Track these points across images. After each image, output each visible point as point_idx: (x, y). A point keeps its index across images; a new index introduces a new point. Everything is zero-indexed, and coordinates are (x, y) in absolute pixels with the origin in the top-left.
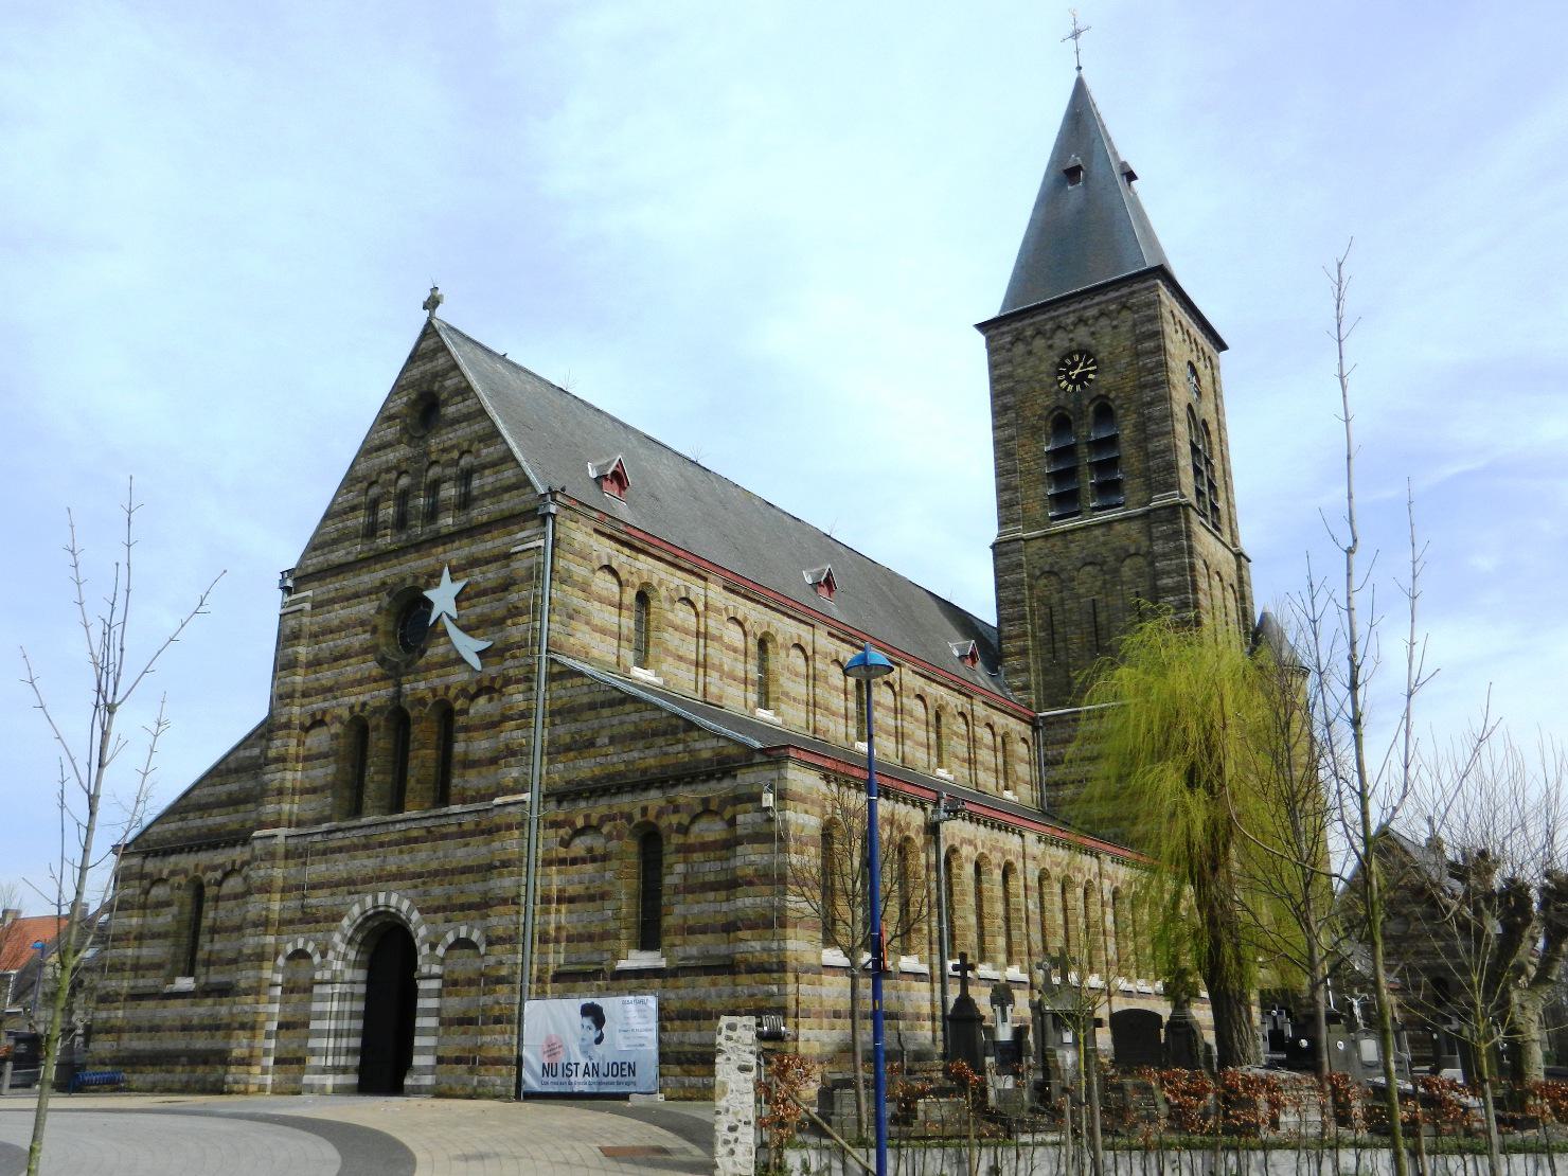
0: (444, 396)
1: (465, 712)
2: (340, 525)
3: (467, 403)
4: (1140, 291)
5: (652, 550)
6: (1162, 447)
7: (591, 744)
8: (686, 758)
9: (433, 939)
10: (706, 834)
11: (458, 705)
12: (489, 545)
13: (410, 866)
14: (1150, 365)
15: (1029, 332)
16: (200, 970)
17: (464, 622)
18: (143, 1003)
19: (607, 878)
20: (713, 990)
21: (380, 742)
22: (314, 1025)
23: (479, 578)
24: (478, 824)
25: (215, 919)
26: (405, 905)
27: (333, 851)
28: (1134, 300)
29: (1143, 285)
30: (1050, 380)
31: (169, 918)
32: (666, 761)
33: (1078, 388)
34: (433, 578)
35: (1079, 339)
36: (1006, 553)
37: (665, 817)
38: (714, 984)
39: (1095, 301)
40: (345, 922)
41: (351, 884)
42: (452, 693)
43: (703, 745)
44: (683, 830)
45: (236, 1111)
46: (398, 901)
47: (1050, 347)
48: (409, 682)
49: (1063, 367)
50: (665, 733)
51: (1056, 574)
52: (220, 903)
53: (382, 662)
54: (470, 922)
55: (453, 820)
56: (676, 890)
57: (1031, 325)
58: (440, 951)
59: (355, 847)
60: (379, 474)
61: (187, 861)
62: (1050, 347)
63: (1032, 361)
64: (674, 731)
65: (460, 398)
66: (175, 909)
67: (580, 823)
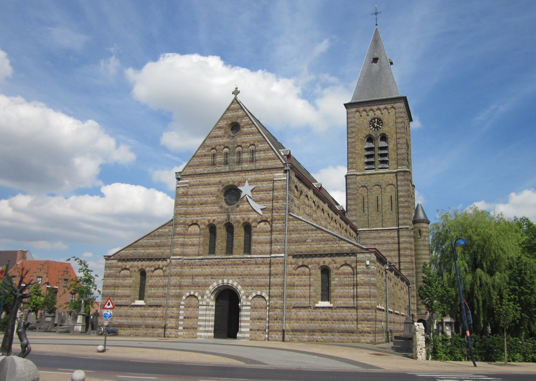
1: (256, 227)
2: (200, 160)
6: (402, 153)
8: (339, 248)
9: (247, 294)
11: (253, 224)
12: (263, 176)
14: (400, 127)
16: (146, 298)
17: (254, 198)
18: (122, 308)
21: (221, 233)
22: (199, 318)
23: (260, 185)
32: (332, 249)
34: (242, 183)
35: (378, 114)
36: (351, 178)
40: (211, 287)
41: (212, 276)
43: (345, 245)
44: (338, 268)
48: (233, 215)
49: (372, 123)
51: (366, 187)
53: (221, 207)
56: (336, 285)
58: (250, 298)
59: (213, 265)
61: (140, 264)
62: (368, 115)
63: (362, 119)
65: (249, 126)
66: (133, 278)
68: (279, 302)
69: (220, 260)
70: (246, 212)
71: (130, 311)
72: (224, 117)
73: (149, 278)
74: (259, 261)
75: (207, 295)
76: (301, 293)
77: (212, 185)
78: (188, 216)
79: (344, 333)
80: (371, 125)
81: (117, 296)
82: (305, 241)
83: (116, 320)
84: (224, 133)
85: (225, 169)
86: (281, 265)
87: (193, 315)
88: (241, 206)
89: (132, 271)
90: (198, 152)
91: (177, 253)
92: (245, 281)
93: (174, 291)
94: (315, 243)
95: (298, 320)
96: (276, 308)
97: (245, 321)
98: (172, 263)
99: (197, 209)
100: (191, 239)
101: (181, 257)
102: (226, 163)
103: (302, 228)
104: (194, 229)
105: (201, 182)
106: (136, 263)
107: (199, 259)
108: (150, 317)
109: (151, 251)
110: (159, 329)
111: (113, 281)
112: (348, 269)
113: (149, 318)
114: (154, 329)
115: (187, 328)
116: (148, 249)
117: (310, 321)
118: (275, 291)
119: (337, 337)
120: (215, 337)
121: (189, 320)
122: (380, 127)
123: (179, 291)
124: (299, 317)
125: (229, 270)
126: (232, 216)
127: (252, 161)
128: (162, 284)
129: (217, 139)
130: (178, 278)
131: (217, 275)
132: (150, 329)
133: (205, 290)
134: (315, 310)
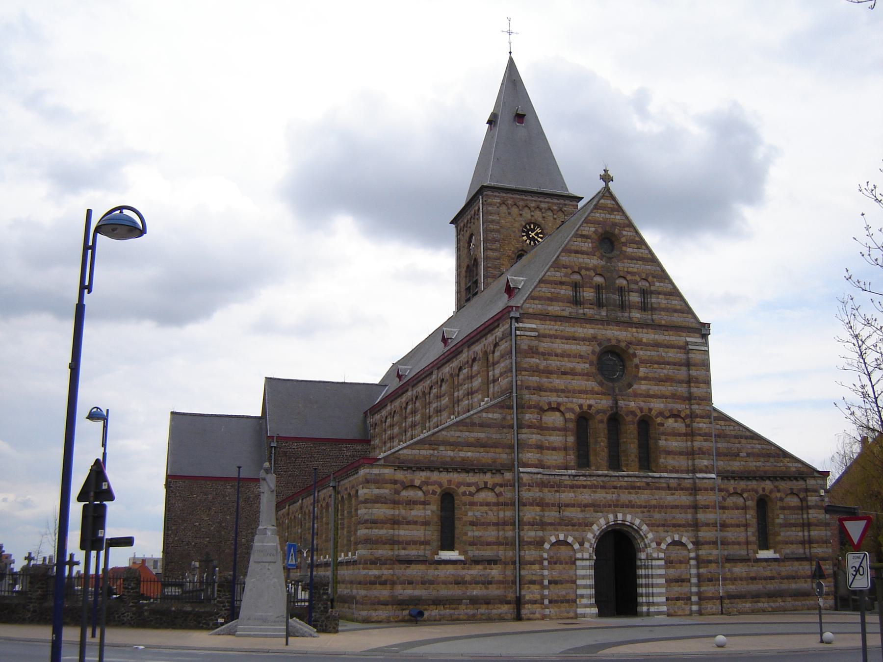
0: (623, 240)
1: (662, 425)
2: (553, 290)
4: (569, 205)
8: (784, 469)
9: (658, 540)
12: (667, 338)
13: (637, 501)
18: (413, 566)
24: (679, 485)
27: (578, 487)
29: (571, 203)
30: (519, 234)
31: (429, 512)
35: (536, 217)
38: (801, 565)
39: (546, 200)
40: (595, 527)
41: (596, 507)
42: (654, 413)
44: (781, 499)
45: (261, 647)
50: (774, 457)
55: (663, 480)
58: (663, 546)
59: (596, 487)
61: (444, 477)
65: (635, 246)
67: (732, 491)
68: (715, 553)
69: (607, 478)
70: (645, 397)
71: (431, 572)
72: (590, 218)
73: (468, 507)
74: (673, 483)
75: (589, 541)
76: (733, 537)
77: (581, 340)
78: (542, 393)
79: (797, 596)
80: (524, 234)
81: (398, 543)
82: (738, 455)
83: (401, 591)
84: (593, 248)
85: (600, 314)
86: (712, 492)
87: (565, 577)
88: (635, 386)
89: (428, 491)
90: (547, 274)
91: (530, 462)
92: (653, 518)
93: (532, 534)
94: (752, 459)
95: (734, 580)
96: (710, 562)
97: (585, 587)
98: (522, 479)
99: (558, 382)
100: (548, 437)
101: (541, 470)
102: (599, 304)
103: (733, 433)
104: (553, 419)
105: (559, 333)
106: (435, 476)
107: (569, 475)
108: (477, 583)
109: (469, 454)
110: (500, 606)
111: (391, 512)
112: (794, 501)
113: (474, 585)
114: (490, 606)
115: (556, 602)
116: (461, 451)
117: (750, 581)
118: (705, 534)
119: (790, 602)
120: (601, 614)
121: (559, 586)
122: (539, 239)
123: (540, 533)
124: (735, 575)
125: (625, 497)
126: (622, 402)
127: (644, 307)
128: (494, 520)
129: (579, 255)
130: (538, 509)
131: (605, 506)
132: (481, 606)
133: (585, 531)
134: (755, 564)
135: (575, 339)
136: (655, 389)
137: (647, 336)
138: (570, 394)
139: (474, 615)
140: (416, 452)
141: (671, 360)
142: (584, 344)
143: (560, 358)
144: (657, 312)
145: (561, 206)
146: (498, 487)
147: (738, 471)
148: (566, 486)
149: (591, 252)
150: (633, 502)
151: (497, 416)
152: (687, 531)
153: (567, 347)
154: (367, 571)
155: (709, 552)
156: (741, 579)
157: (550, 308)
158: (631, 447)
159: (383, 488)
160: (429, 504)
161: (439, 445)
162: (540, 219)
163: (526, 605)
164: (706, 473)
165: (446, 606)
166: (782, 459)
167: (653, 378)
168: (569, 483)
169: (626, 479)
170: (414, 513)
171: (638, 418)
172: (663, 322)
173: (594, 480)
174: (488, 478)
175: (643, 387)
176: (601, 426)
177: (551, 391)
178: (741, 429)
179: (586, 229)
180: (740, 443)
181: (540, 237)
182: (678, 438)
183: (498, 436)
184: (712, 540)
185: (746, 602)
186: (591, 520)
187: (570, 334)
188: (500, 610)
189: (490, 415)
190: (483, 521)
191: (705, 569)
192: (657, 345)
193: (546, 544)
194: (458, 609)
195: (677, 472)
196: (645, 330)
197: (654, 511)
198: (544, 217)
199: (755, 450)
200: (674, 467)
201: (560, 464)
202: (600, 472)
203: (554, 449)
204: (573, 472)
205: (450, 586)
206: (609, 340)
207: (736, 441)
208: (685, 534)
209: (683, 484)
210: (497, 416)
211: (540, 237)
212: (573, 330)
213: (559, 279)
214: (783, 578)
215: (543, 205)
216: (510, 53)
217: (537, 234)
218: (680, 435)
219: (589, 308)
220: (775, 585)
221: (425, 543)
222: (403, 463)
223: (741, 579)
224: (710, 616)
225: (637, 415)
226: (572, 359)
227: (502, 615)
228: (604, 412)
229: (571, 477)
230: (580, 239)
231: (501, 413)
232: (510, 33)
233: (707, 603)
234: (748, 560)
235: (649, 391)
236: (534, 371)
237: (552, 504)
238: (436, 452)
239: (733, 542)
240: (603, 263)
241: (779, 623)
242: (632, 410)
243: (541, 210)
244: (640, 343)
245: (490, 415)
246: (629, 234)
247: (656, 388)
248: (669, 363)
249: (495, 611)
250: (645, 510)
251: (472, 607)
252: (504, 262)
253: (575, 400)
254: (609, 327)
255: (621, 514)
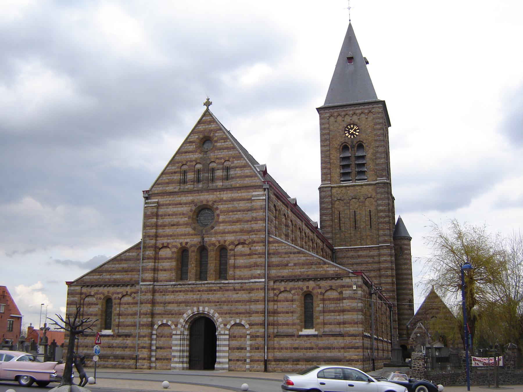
0: (215, 139)
2: (170, 177)
3: (226, 143)
4: (376, 107)
5: (282, 199)
7: (287, 265)
8: (323, 272)
9: (225, 323)
10: (330, 296)
12: (240, 195)
15: (335, 114)
18: (88, 338)
19: (294, 307)
20: (335, 341)
24: (241, 287)
25: (119, 311)
26: (212, 311)
28: (373, 110)
29: (377, 106)
31: (97, 309)
33: (352, 137)
37: (315, 290)
38: (336, 339)
40: (185, 315)
41: (187, 303)
42: (227, 243)
46: (209, 310)
47: (343, 121)
50: (316, 264)
52: (121, 306)
54: (241, 318)
55: (231, 285)
57: (336, 111)
58: (228, 326)
59: (187, 291)
60: (187, 162)
61: (105, 290)
63: (336, 125)
64: (319, 264)
65: (223, 141)
69: (194, 285)
70: (222, 234)
73: (117, 305)
74: (238, 286)
75: (181, 323)
84: (196, 148)
87: (166, 345)
88: (216, 228)
94: (297, 267)
103: (284, 251)
105: (171, 202)
106: (101, 289)
107: (171, 285)
108: (119, 347)
109: (118, 276)
110: (129, 360)
114: (124, 360)
115: (161, 359)
124: (282, 346)
125: (205, 296)
132: (120, 360)
134: (298, 338)
135: (180, 204)
136: (229, 228)
137: (226, 195)
138: (175, 237)
139: (115, 365)
140: (91, 277)
141: (241, 208)
142: (186, 207)
143: (171, 217)
144: (234, 180)
145: (370, 109)
146: (133, 294)
147: (287, 276)
148: (169, 292)
149: (194, 150)
150: (210, 299)
151: (134, 254)
152: (245, 317)
153: (175, 209)
154: (65, 340)
155: (257, 330)
156: (286, 349)
157: (167, 188)
158: (212, 265)
159: (75, 297)
160: (97, 305)
161: (103, 272)
162: (357, 121)
163: (139, 361)
164: (259, 278)
165: (102, 360)
166: (322, 265)
167: (228, 221)
168: (171, 289)
169: (206, 285)
170: (91, 309)
171: (208, 246)
172: (238, 185)
173: (186, 287)
174: (129, 289)
175: (221, 228)
176: (193, 254)
177: (164, 236)
178: (290, 247)
179: (193, 137)
180: (289, 257)
181: (357, 132)
182: (244, 257)
183: (134, 265)
184: (259, 322)
185: (288, 364)
186: (182, 311)
187: (178, 202)
188: (129, 363)
189: (131, 254)
190: (125, 313)
191: (254, 341)
192: (233, 200)
193: (155, 325)
194: (108, 361)
195: (242, 279)
196: (225, 192)
197: (224, 304)
198: (359, 119)
199: (300, 261)
200: (240, 276)
201: (168, 279)
202: (190, 282)
203: (165, 270)
204: (174, 283)
205: (106, 349)
206: (202, 202)
207: (287, 256)
208: (244, 318)
209: (244, 287)
210: (134, 254)
211: (357, 132)
212: (180, 199)
213: (174, 171)
214: (320, 349)
215: (357, 112)
216: (350, 20)
217: (355, 130)
218: (245, 255)
219: (190, 185)
220: (313, 354)
221: (294, 324)
222: (85, 283)
223: (286, 349)
224: (255, 372)
225: (209, 247)
226: (178, 216)
227: (130, 366)
228: (195, 245)
229: (173, 286)
230: (188, 144)
231: (137, 252)
232: (349, 8)
233: (253, 363)
234: (293, 336)
235: (225, 230)
236: (153, 226)
237: (160, 302)
238: (101, 276)
239: (282, 323)
240: (201, 156)
241: (228, 377)
242: (213, 242)
243: (356, 114)
244: (221, 201)
245: (131, 254)
246: (220, 134)
247: (230, 227)
248: (239, 211)
249: (126, 363)
250: (218, 304)
251: (115, 360)
252: (333, 152)
253: (178, 240)
254: (202, 194)
255: (202, 307)
